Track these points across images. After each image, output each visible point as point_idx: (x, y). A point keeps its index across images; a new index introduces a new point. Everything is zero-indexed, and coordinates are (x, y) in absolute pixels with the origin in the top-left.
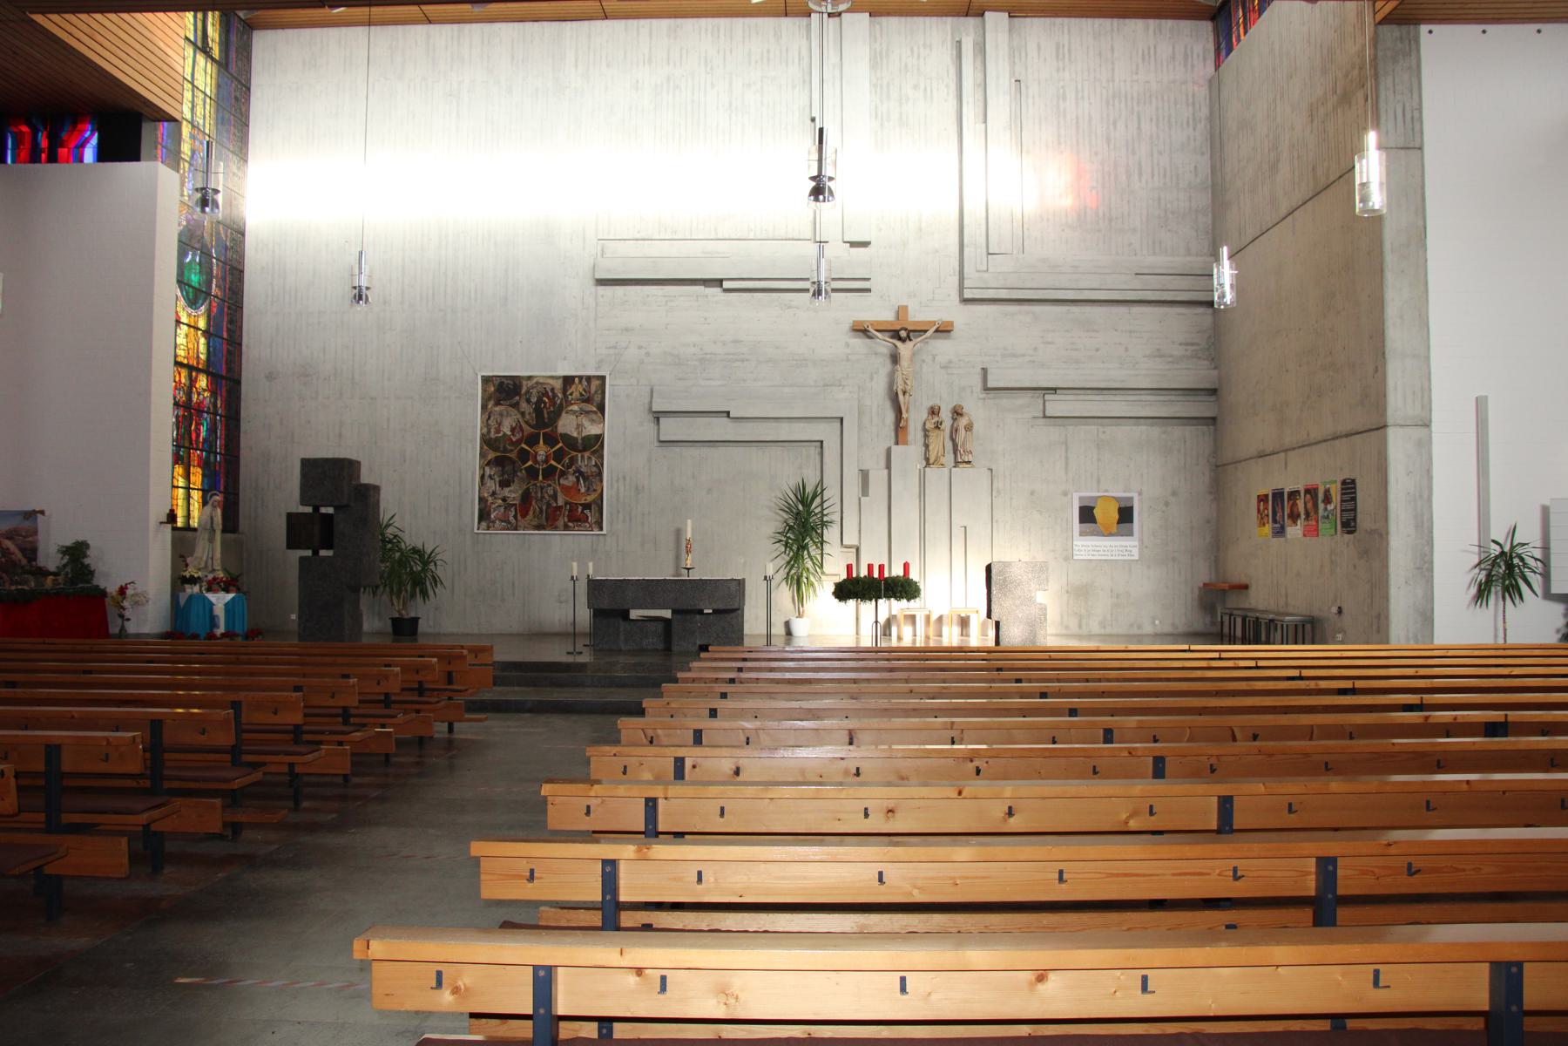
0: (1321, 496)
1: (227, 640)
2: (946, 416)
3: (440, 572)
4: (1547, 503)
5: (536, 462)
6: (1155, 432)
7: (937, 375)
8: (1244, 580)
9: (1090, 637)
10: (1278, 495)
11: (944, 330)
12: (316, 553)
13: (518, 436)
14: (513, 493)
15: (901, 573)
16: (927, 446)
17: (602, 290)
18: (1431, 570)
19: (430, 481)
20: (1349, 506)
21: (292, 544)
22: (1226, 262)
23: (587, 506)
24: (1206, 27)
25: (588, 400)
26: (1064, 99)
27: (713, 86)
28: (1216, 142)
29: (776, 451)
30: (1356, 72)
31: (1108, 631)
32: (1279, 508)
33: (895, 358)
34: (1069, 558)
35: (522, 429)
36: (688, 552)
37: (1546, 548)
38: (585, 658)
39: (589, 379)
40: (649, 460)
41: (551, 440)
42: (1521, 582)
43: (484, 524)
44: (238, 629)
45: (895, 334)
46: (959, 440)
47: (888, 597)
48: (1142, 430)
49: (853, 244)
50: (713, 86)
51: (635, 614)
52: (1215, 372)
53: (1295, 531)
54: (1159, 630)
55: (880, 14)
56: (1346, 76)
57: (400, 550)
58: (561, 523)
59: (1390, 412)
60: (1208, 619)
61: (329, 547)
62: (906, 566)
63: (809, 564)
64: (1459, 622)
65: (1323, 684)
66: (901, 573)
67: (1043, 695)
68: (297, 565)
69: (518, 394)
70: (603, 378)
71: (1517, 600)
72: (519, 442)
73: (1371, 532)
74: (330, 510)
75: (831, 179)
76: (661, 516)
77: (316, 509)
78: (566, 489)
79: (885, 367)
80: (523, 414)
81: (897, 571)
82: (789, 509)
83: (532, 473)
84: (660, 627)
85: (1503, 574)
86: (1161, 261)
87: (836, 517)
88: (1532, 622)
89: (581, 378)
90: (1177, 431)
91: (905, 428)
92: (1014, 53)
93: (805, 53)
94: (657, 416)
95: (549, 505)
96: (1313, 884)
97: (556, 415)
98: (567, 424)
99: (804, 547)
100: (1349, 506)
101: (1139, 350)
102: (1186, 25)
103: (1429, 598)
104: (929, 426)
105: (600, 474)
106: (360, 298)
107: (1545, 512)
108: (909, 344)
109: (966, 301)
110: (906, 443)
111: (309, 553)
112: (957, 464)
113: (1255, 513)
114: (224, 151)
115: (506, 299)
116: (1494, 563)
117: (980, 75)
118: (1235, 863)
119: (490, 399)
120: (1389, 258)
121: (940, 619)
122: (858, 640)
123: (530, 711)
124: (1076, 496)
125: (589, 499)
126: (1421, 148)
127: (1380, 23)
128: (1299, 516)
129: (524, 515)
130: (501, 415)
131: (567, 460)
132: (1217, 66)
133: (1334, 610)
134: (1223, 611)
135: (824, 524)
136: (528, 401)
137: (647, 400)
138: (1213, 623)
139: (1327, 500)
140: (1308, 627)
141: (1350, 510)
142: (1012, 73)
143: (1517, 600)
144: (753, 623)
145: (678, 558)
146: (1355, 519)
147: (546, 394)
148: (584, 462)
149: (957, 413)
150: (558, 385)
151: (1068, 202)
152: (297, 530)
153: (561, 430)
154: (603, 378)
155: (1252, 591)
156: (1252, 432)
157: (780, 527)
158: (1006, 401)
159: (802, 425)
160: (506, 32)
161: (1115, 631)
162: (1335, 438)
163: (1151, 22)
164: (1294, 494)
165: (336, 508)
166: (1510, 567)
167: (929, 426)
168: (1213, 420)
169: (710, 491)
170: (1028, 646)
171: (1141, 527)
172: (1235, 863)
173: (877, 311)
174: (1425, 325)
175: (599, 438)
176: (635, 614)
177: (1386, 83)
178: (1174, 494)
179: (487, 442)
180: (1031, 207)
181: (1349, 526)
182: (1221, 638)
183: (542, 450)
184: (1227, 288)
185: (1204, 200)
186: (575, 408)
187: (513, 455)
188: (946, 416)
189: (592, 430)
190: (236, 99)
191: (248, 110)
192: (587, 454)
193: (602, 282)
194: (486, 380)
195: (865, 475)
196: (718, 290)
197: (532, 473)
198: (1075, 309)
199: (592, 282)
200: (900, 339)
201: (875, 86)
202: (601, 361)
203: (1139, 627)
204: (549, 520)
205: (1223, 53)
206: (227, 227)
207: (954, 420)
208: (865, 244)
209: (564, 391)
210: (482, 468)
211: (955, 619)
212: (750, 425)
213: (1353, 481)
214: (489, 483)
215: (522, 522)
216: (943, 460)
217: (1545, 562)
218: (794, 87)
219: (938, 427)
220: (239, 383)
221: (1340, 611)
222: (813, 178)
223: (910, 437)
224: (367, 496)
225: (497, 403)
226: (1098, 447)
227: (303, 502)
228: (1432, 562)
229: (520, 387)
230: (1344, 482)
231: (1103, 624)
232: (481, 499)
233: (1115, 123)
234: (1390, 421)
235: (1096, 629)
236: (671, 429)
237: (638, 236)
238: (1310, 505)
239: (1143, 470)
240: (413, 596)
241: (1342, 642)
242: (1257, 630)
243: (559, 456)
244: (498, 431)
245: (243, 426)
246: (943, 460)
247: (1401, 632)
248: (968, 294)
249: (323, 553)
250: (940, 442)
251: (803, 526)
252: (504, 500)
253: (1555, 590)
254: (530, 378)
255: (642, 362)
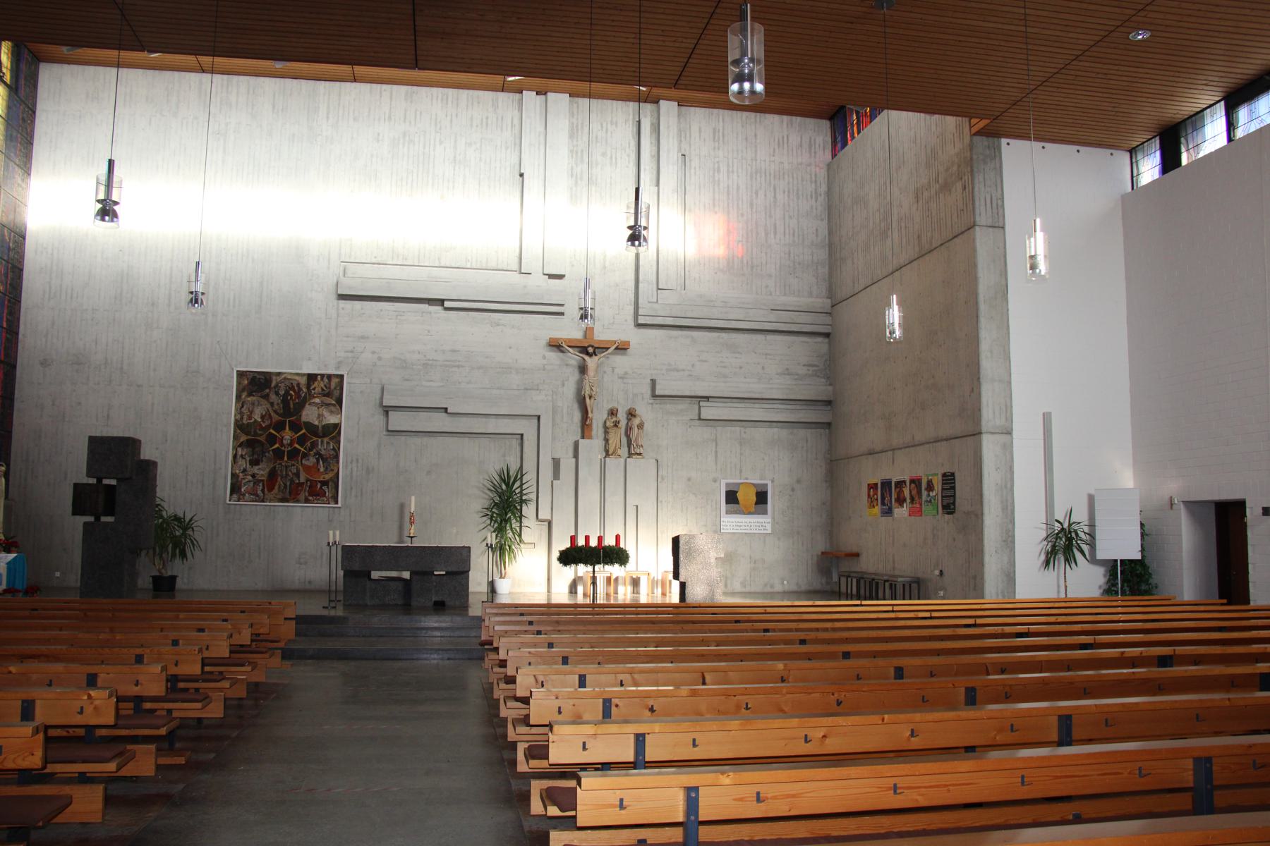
0: (924, 485)
1: (9, 596)
2: (622, 416)
3: (197, 535)
4: (1092, 492)
5: (282, 445)
6: (784, 433)
7: (616, 384)
8: (855, 550)
9: (733, 594)
10: (886, 484)
11: (622, 348)
12: (97, 519)
13: (268, 422)
14: (262, 471)
15: (613, 543)
16: (607, 440)
17: (342, 303)
18: (1013, 542)
19: (195, 458)
20: (949, 493)
21: (76, 512)
22: (896, 307)
23: (325, 483)
24: (825, 124)
25: (328, 395)
26: (719, 171)
27: (441, 143)
28: (833, 210)
29: (485, 441)
30: (955, 168)
31: (748, 589)
32: (887, 494)
33: (583, 369)
34: (718, 530)
35: (270, 417)
36: (412, 523)
37: (1092, 526)
38: (339, 612)
39: (330, 377)
40: (379, 446)
41: (295, 427)
42: (1076, 551)
43: (235, 496)
44: (19, 586)
45: (584, 350)
46: (633, 437)
47: (606, 563)
48: (775, 431)
49: (551, 276)
50: (441, 143)
51: (375, 575)
52: (830, 388)
53: (901, 512)
54: (787, 588)
55: (578, 96)
56: (947, 170)
57: (162, 517)
58: (302, 496)
59: (983, 423)
60: (824, 581)
61: (111, 514)
62: (618, 537)
63: (510, 535)
64: (1034, 582)
65: (1008, 629)
66: (613, 543)
67: (803, 642)
68: (81, 528)
69: (269, 387)
70: (342, 377)
71: (1073, 565)
72: (268, 427)
73: (968, 513)
74: (113, 482)
75: (645, 228)
76: (393, 493)
77: (100, 480)
78: (307, 469)
79: (574, 376)
80: (272, 404)
81: (609, 541)
82: (495, 489)
83: (278, 454)
84: (400, 585)
85: (1064, 544)
86: (792, 300)
87: (533, 496)
88: (1085, 581)
89: (322, 376)
90: (802, 432)
91: (590, 426)
92: (682, 134)
93: (516, 122)
94: (387, 410)
95: (292, 481)
96: (1191, 778)
97: (301, 406)
98: (310, 414)
99: (507, 521)
100: (949, 493)
101: (771, 369)
102: (810, 122)
103: (1012, 563)
104: (609, 424)
105: (337, 457)
106: (196, 302)
107: (1091, 499)
108: (595, 358)
109: (639, 325)
110: (590, 437)
111: (91, 519)
112: (630, 455)
113: (865, 497)
114: (11, 164)
115: (260, 307)
116: (1057, 537)
117: (655, 148)
118: (1139, 764)
119: (243, 390)
120: (983, 307)
121: (617, 579)
122: (549, 597)
123: (311, 657)
124: (723, 483)
125: (327, 477)
126: (1003, 228)
127: (978, 133)
128: (905, 500)
129: (271, 489)
130: (253, 404)
131: (308, 444)
132: (834, 155)
133: (937, 572)
134: (837, 571)
135: (522, 502)
136: (277, 394)
137: (378, 396)
138: (828, 583)
139: (930, 487)
140: (914, 586)
141: (951, 496)
142: (680, 150)
143: (1073, 565)
144: (477, 583)
145: (401, 528)
146: (954, 504)
147: (292, 388)
148: (324, 446)
149: (631, 414)
150: (303, 381)
151: (720, 251)
152: (83, 499)
153: (304, 419)
154: (342, 377)
155: (863, 558)
156: (866, 434)
157: (487, 504)
158: (669, 406)
159: (506, 421)
160: (269, 85)
161: (753, 590)
162: (937, 441)
163: (785, 117)
164: (900, 484)
165: (118, 480)
166: (1070, 540)
167: (609, 424)
168: (829, 425)
169: (429, 473)
170: (708, 602)
171: (774, 506)
172: (1139, 764)
173: (570, 330)
174: (1007, 358)
175: (337, 427)
176: (375, 575)
177: (979, 178)
178: (798, 481)
179: (239, 426)
180: (691, 252)
181: (949, 508)
182: (839, 595)
183: (287, 435)
184: (896, 326)
185: (823, 254)
186: (317, 400)
187: (262, 439)
188: (622, 416)
189: (332, 420)
190: (24, 120)
191: (33, 130)
192: (326, 440)
193: (342, 297)
194: (241, 374)
195: (556, 463)
196: (439, 308)
197: (278, 454)
198: (724, 335)
199: (335, 296)
200: (588, 354)
201: (572, 151)
202: (340, 363)
203: (772, 586)
204: (292, 494)
205: (839, 145)
206: (11, 230)
207: (629, 420)
208: (561, 277)
209: (308, 388)
210: (235, 448)
211: (628, 581)
212: (464, 419)
213: (953, 474)
214: (242, 463)
215: (269, 495)
216: (619, 452)
217: (1092, 535)
218: (507, 148)
219: (616, 425)
220: (14, 367)
221: (941, 573)
222: (630, 228)
223: (594, 433)
224: (147, 469)
225: (250, 395)
226: (741, 444)
227: (89, 475)
228: (1014, 536)
229: (270, 381)
230: (944, 475)
231: (743, 584)
232: (233, 475)
233: (757, 193)
234: (984, 429)
235: (738, 588)
236: (398, 421)
237: (374, 260)
238: (914, 492)
239: (774, 463)
240: (174, 555)
241: (943, 598)
242: (871, 587)
243: (301, 441)
244: (250, 418)
245: (17, 404)
246: (619, 452)
247: (992, 590)
248: (641, 320)
249: (104, 519)
250: (617, 437)
251: (506, 506)
252: (253, 476)
253: (1099, 557)
254: (279, 374)
255: (375, 365)
